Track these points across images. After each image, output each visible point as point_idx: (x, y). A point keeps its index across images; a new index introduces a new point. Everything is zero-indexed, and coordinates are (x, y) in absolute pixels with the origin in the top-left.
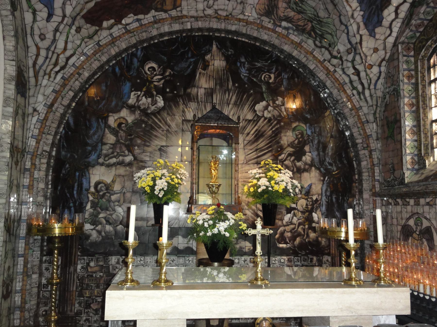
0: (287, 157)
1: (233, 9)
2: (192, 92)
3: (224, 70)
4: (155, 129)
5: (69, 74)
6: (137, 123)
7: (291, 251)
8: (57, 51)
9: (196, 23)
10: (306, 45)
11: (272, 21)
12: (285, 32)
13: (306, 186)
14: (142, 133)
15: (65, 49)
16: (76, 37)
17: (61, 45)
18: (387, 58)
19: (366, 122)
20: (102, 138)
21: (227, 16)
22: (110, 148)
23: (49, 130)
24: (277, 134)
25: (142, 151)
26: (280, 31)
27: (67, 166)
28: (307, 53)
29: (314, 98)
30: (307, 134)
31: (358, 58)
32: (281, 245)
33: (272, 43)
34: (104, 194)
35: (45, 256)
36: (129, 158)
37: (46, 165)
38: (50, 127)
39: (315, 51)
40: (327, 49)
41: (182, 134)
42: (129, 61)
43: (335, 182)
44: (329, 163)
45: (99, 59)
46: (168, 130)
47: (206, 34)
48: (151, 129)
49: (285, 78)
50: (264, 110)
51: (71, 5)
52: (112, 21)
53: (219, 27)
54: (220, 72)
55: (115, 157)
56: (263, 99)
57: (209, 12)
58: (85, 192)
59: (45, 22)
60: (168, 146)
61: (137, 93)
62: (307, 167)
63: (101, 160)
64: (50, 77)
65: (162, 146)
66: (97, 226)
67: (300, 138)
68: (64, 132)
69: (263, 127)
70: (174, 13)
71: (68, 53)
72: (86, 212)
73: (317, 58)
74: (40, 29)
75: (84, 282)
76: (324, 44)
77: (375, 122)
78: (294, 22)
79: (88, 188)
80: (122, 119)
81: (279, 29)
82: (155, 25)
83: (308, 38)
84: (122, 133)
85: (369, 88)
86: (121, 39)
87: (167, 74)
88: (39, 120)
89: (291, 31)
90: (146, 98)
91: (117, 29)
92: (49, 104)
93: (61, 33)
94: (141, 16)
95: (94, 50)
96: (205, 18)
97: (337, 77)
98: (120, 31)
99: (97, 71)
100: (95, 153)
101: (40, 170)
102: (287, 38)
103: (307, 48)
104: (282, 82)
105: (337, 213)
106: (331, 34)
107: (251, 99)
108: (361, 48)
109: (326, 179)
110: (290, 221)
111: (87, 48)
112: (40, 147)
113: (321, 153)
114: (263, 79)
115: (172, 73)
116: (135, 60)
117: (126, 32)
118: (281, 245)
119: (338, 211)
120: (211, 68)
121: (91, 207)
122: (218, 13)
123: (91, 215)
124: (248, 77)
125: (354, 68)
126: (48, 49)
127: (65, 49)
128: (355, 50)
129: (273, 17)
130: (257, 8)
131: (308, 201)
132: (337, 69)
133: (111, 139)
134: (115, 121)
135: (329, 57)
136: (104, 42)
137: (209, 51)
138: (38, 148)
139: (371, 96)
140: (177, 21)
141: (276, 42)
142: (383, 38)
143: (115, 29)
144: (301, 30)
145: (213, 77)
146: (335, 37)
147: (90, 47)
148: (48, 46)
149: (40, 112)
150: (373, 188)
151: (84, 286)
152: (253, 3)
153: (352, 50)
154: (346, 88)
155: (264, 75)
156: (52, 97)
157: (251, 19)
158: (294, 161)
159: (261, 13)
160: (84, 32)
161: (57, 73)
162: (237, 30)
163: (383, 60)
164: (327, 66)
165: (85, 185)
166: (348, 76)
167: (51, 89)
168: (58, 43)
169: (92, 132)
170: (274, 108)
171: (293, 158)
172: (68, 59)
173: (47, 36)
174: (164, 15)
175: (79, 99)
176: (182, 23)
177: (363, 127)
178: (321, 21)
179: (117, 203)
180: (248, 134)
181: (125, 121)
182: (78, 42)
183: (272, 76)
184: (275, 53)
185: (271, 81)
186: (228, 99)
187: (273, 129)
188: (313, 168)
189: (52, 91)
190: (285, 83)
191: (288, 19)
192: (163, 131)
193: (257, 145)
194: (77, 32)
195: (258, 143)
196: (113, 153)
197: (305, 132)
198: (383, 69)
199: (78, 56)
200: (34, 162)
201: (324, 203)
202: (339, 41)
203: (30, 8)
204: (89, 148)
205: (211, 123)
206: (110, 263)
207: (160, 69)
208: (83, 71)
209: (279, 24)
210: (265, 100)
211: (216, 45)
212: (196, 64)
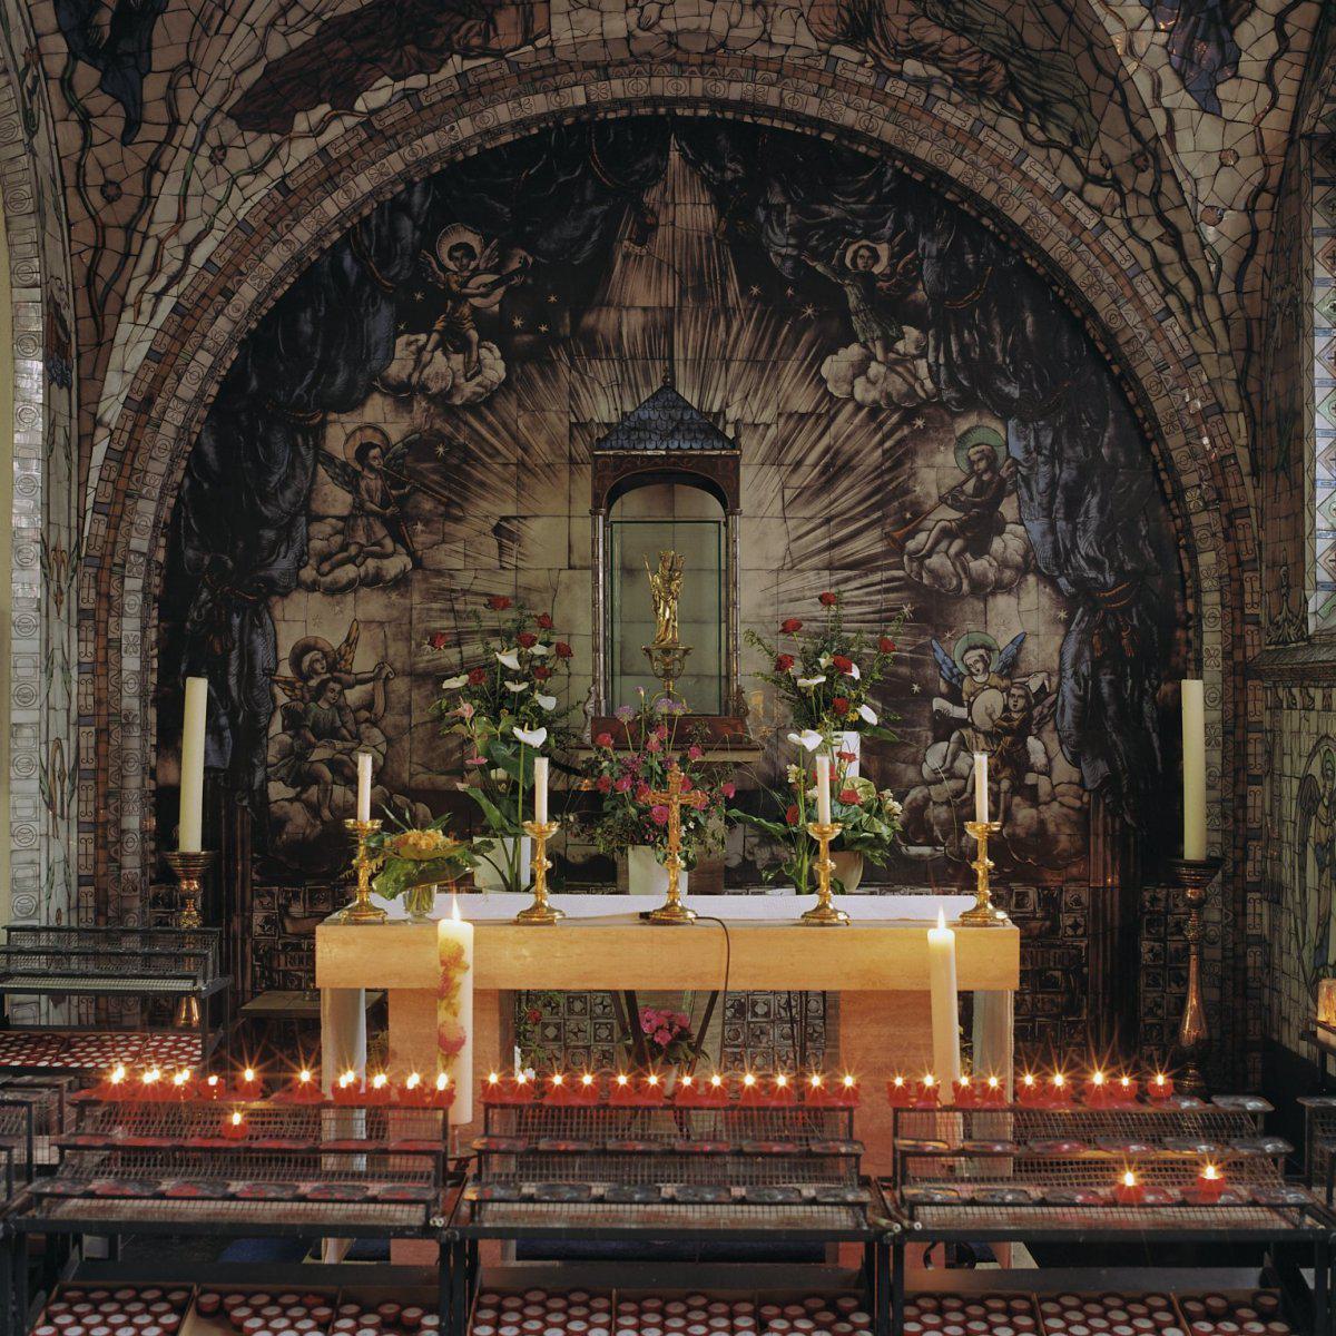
0: (937, 543)
1: (730, 27)
2: (601, 326)
3: (708, 240)
6: (419, 445)
10: (995, 135)
13: (1003, 641)
14: (435, 477)
15: (181, 220)
18: (1273, 181)
20: (308, 499)
24: (899, 458)
27: (204, 595)
28: (998, 167)
29: (1036, 323)
30: (1008, 456)
31: (1167, 184)
32: (914, 850)
33: (875, 135)
34: (324, 683)
36: (397, 564)
37: (140, 596)
39: (1029, 160)
40: (1066, 151)
41: (571, 473)
42: (384, 230)
43: (1111, 626)
44: (1087, 558)
45: (289, 236)
46: (521, 464)
47: (642, 111)
49: (929, 257)
50: (855, 376)
51: (194, 87)
52: (325, 109)
55: (350, 560)
56: (849, 338)
58: (262, 680)
59: (116, 145)
60: (525, 518)
62: (1008, 574)
63: (308, 574)
64: (138, 313)
66: (304, 790)
67: (985, 471)
68: (187, 483)
71: (190, 231)
72: (271, 743)
74: (103, 169)
75: (275, 964)
76: (1056, 135)
77: (1242, 410)
79: (272, 666)
80: (369, 432)
81: (896, 87)
82: (466, 106)
83: (999, 114)
85: (1215, 292)
86: (354, 165)
87: (515, 265)
88: (112, 455)
89: (938, 91)
90: (445, 353)
92: (139, 398)
93: (166, 174)
95: (271, 207)
96: (632, 66)
97: (1110, 248)
98: (350, 134)
99: (282, 274)
103: (1001, 150)
106: (1071, 102)
107: (806, 338)
108: (1175, 152)
109: (1078, 616)
110: (948, 765)
111: (249, 204)
113: (1061, 524)
114: (848, 262)
115: (530, 260)
116: (406, 224)
118: (914, 850)
120: (664, 233)
121: (285, 729)
122: (677, 46)
123: (287, 752)
124: (796, 259)
125: (1161, 217)
126: (129, 228)
127: (181, 220)
128: (1156, 158)
129: (871, 45)
130: (813, 18)
132: (1110, 222)
133: (335, 499)
134: (349, 437)
135: (1075, 178)
136: (302, 179)
137: (658, 173)
139: (1225, 318)
140: (538, 84)
141: (888, 132)
142: (1246, 114)
143: (335, 129)
144: (973, 89)
146: (1086, 114)
148: (128, 218)
150: (1233, 647)
151: (275, 976)
152: (797, 4)
153: (1146, 160)
154: (1143, 286)
155: (855, 247)
158: (959, 554)
161: (159, 296)
162: (749, 98)
163: (1261, 189)
164: (1072, 210)
165: (262, 657)
166: (1147, 244)
167: (144, 348)
168: (157, 211)
170: (891, 366)
171: (957, 545)
172: (190, 248)
173: (126, 187)
176: (557, 90)
178: (1037, 62)
179: (364, 714)
180: (798, 464)
181: (379, 436)
182: (219, 192)
183: (883, 250)
184: (893, 166)
185: (877, 270)
186: (724, 345)
187: (888, 444)
188: (1031, 579)
189: (146, 357)
190: (929, 272)
191: (919, 51)
192: (505, 465)
193: (831, 503)
194: (214, 164)
195: (833, 496)
196: (344, 547)
197: (1001, 452)
198: (1263, 219)
200: (104, 586)
201: (1070, 700)
202: (1103, 127)
203: (71, 109)
205: (646, 449)
207: (488, 251)
208: (240, 283)
210: (856, 340)
211: (681, 149)
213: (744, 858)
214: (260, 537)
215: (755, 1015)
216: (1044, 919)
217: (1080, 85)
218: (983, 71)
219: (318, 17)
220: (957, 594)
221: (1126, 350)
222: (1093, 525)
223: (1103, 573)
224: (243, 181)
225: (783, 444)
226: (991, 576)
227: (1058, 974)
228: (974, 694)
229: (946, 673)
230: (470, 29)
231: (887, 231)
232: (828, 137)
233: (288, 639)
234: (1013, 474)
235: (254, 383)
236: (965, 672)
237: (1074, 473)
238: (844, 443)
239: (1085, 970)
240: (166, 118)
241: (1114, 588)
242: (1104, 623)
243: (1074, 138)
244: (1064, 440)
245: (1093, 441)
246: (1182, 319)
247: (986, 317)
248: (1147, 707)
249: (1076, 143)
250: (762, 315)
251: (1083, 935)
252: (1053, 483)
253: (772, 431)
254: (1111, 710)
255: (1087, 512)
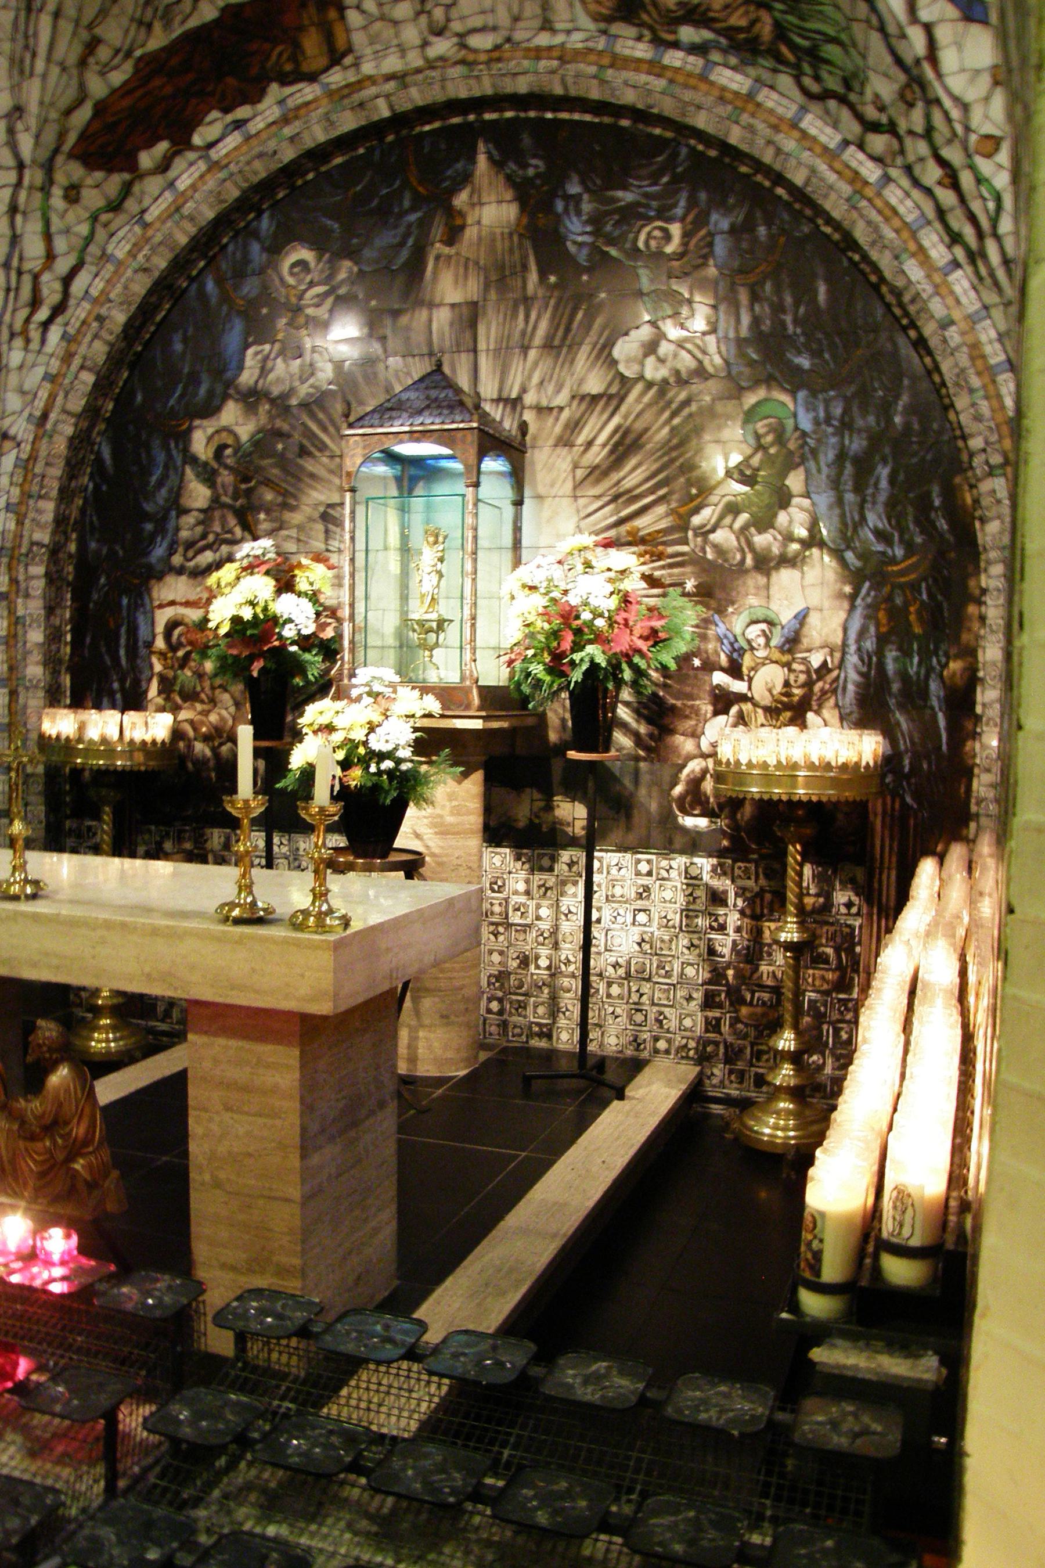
0: (721, 518)
4: (310, 454)
5: (78, 325)
7: (725, 843)
8: (27, 266)
9: (402, 94)
10: (775, 96)
11: (647, 33)
12: (695, 63)
13: (786, 616)
15: (50, 256)
16: (71, 216)
17: (34, 248)
19: (1007, 366)
21: (497, 47)
22: (199, 523)
23: (42, 487)
25: (276, 525)
26: (678, 64)
27: (103, 580)
28: (776, 128)
30: (796, 428)
35: (67, 817)
38: (43, 477)
40: (843, 100)
42: (238, 255)
48: (300, 456)
52: (163, 146)
53: (477, 93)
54: (499, 244)
57: (441, 47)
58: (143, 651)
61: (261, 351)
62: (795, 547)
63: (177, 560)
64: (28, 341)
65: (329, 506)
67: (772, 444)
68: (91, 486)
69: (638, 416)
70: (336, 78)
71: (63, 266)
73: (814, 139)
76: (833, 83)
78: (714, 20)
79: (150, 639)
80: (224, 434)
81: (674, 58)
83: (775, 71)
84: (226, 478)
89: (716, 56)
90: (285, 361)
91: (184, 165)
94: (242, 112)
97: (893, 201)
98: (193, 168)
100: (163, 539)
101: (27, 596)
102: (703, 87)
104: (711, 245)
105: (898, 715)
108: (939, 75)
109: (864, 591)
111: (115, 239)
112: (26, 533)
113: (850, 497)
114: (641, 245)
117: (209, 170)
119: (901, 707)
120: (471, 233)
121: (160, 693)
127: (50, 256)
131: (790, 670)
132: (894, 173)
133: (198, 494)
134: (210, 439)
135: (856, 128)
136: (157, 213)
137: (465, 178)
138: (21, 536)
139: (1006, 262)
145: (477, 263)
147: (121, 234)
149: (19, 438)
155: (647, 229)
156: (43, 395)
157: (576, 41)
158: (744, 529)
159: (604, 11)
160: (92, 199)
161: (46, 325)
162: (536, 89)
164: (854, 164)
165: (143, 633)
166: (929, 192)
167: (40, 371)
169: (154, 479)
171: (744, 517)
172: (67, 280)
174: (308, 92)
175: (122, 388)
177: (991, 387)
180: (589, 444)
182: (84, 229)
183: (676, 229)
184: (688, 146)
185: (669, 249)
186: (523, 333)
187: (676, 421)
195: (622, 474)
196: (204, 536)
197: (790, 423)
199: (94, 269)
204: (149, 527)
206: (208, 845)
209: (670, 37)
211: (488, 153)
212: (424, 225)
213: (531, 820)
214: (142, 530)
215: (538, 967)
216: (817, 895)
217: (838, 16)
218: (753, 23)
219: (129, 54)
220: (741, 569)
221: (912, 309)
222: (882, 497)
223: (892, 548)
224: (104, 217)
225: (575, 426)
226: (776, 550)
227: (829, 951)
228: (754, 669)
229: (727, 647)
230: (280, 55)
231: (679, 211)
232: (625, 123)
233: (163, 617)
234: (802, 447)
235: (139, 398)
236: (746, 646)
237: (865, 443)
238: (634, 421)
239: (858, 949)
240: (11, 162)
241: (903, 561)
242: (889, 599)
243: (847, 83)
244: (855, 409)
245: (886, 410)
246: (969, 269)
247: (778, 289)
248: (934, 686)
249: (848, 87)
250: (560, 299)
251: (858, 914)
252: (841, 456)
253: (566, 414)
254: (896, 687)
255: (876, 485)
